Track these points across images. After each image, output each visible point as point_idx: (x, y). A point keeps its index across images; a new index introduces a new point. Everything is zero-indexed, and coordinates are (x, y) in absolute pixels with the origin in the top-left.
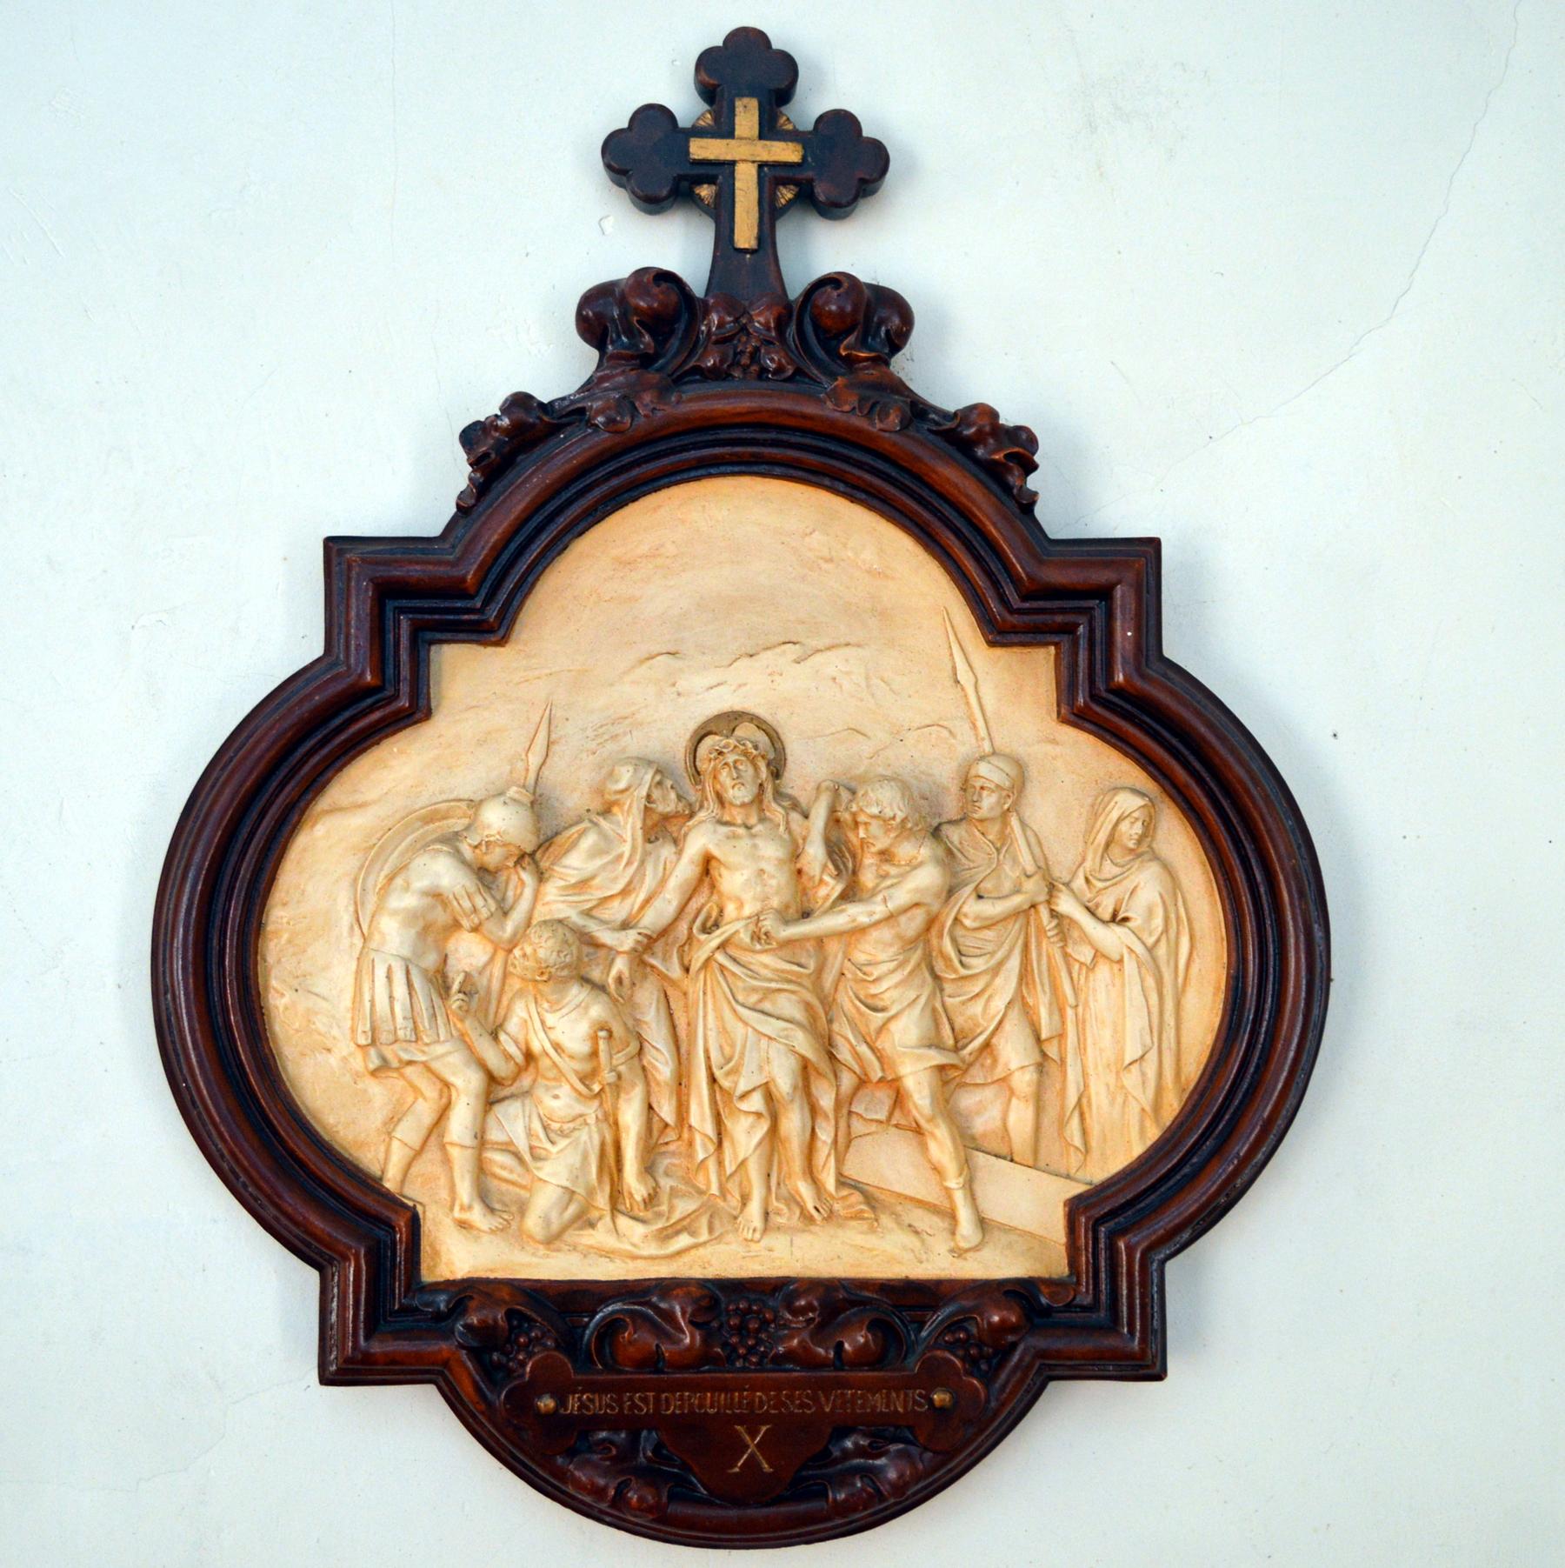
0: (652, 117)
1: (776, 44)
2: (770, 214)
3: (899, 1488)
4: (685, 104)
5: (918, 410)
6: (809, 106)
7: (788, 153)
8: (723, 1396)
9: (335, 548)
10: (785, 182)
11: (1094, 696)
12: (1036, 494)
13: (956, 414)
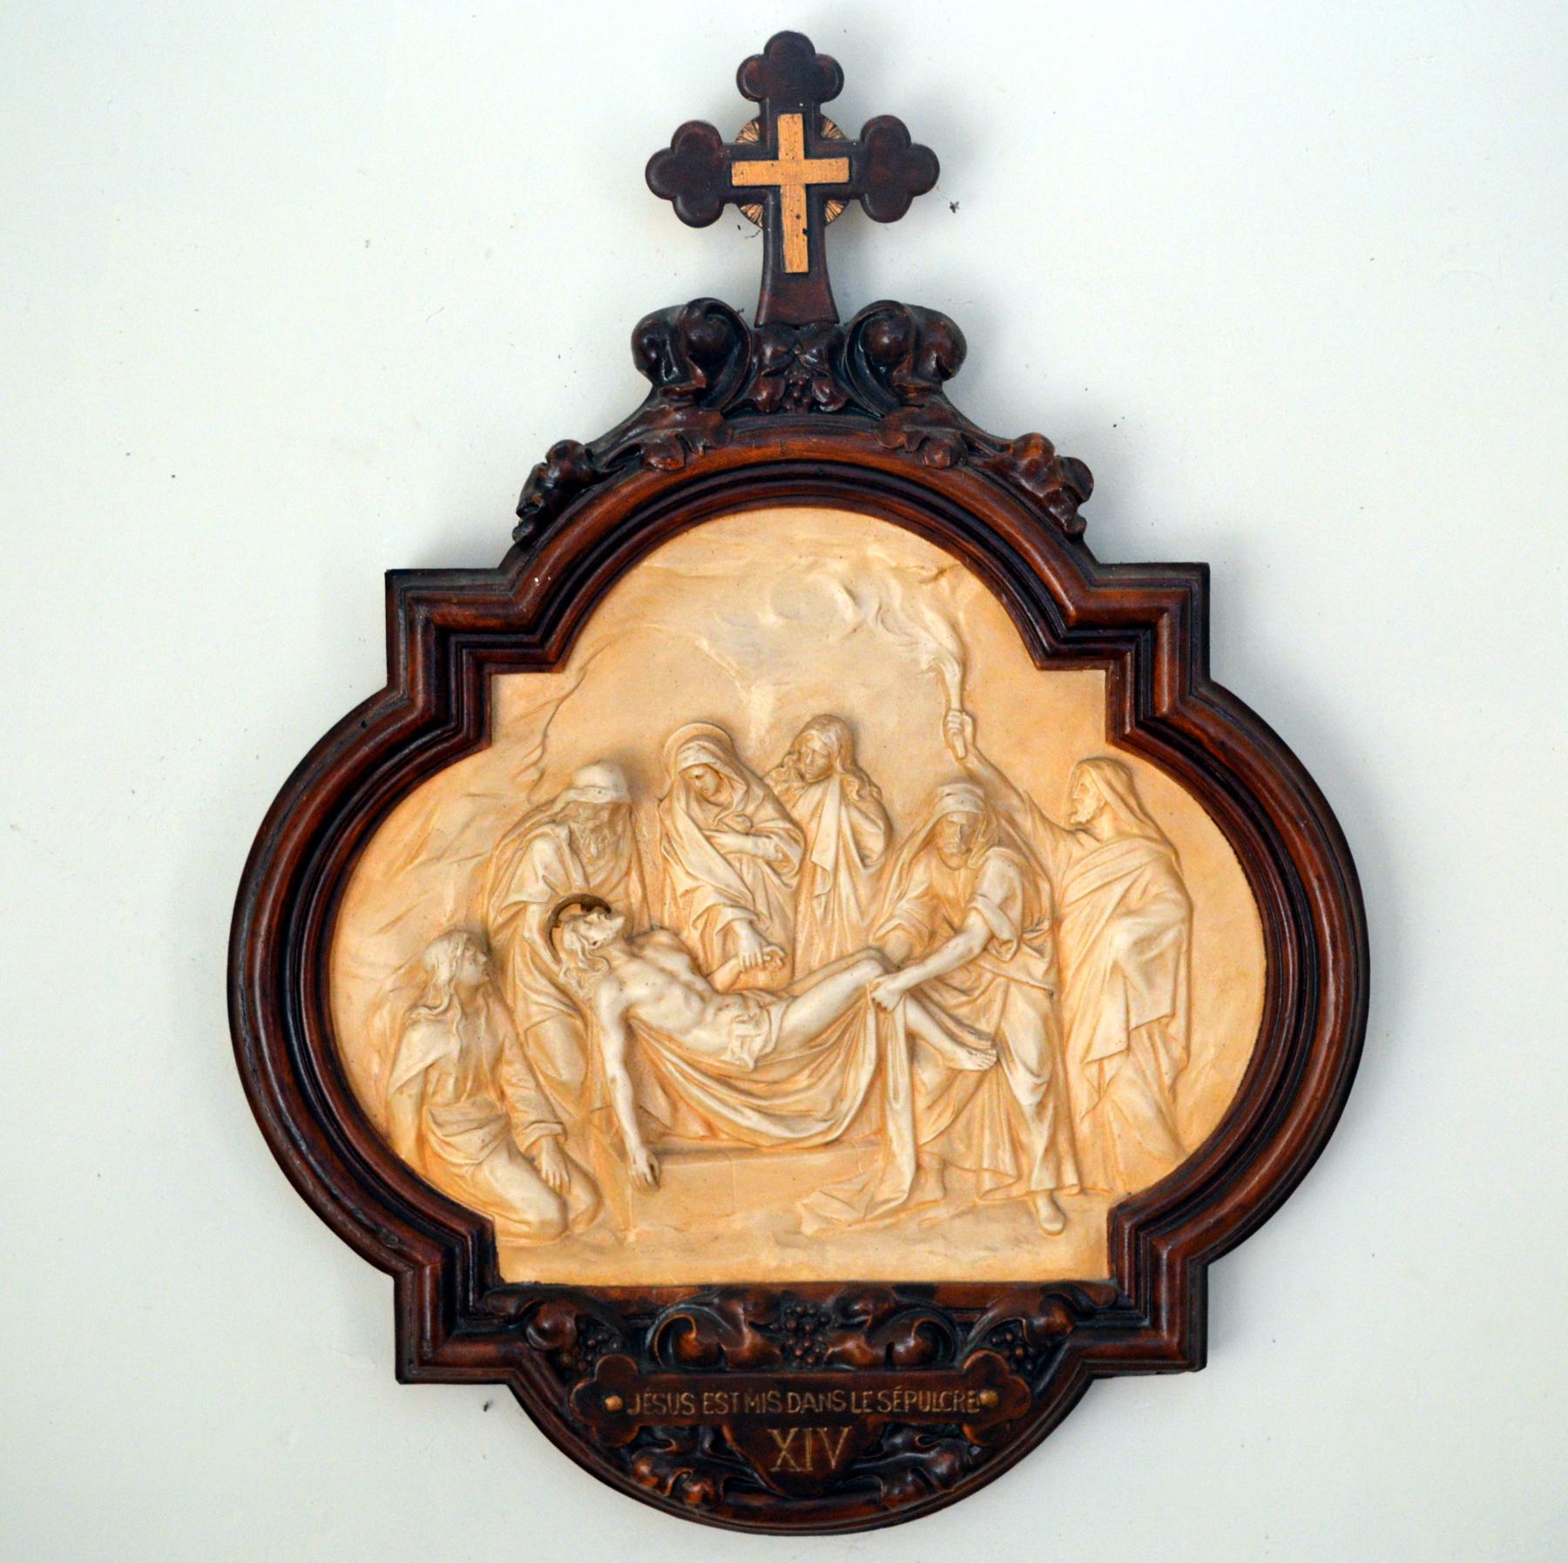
1: (917, 138)
3: (947, 1481)
5: (970, 442)
7: (834, 171)
8: (935, 1395)
11: (1138, 724)
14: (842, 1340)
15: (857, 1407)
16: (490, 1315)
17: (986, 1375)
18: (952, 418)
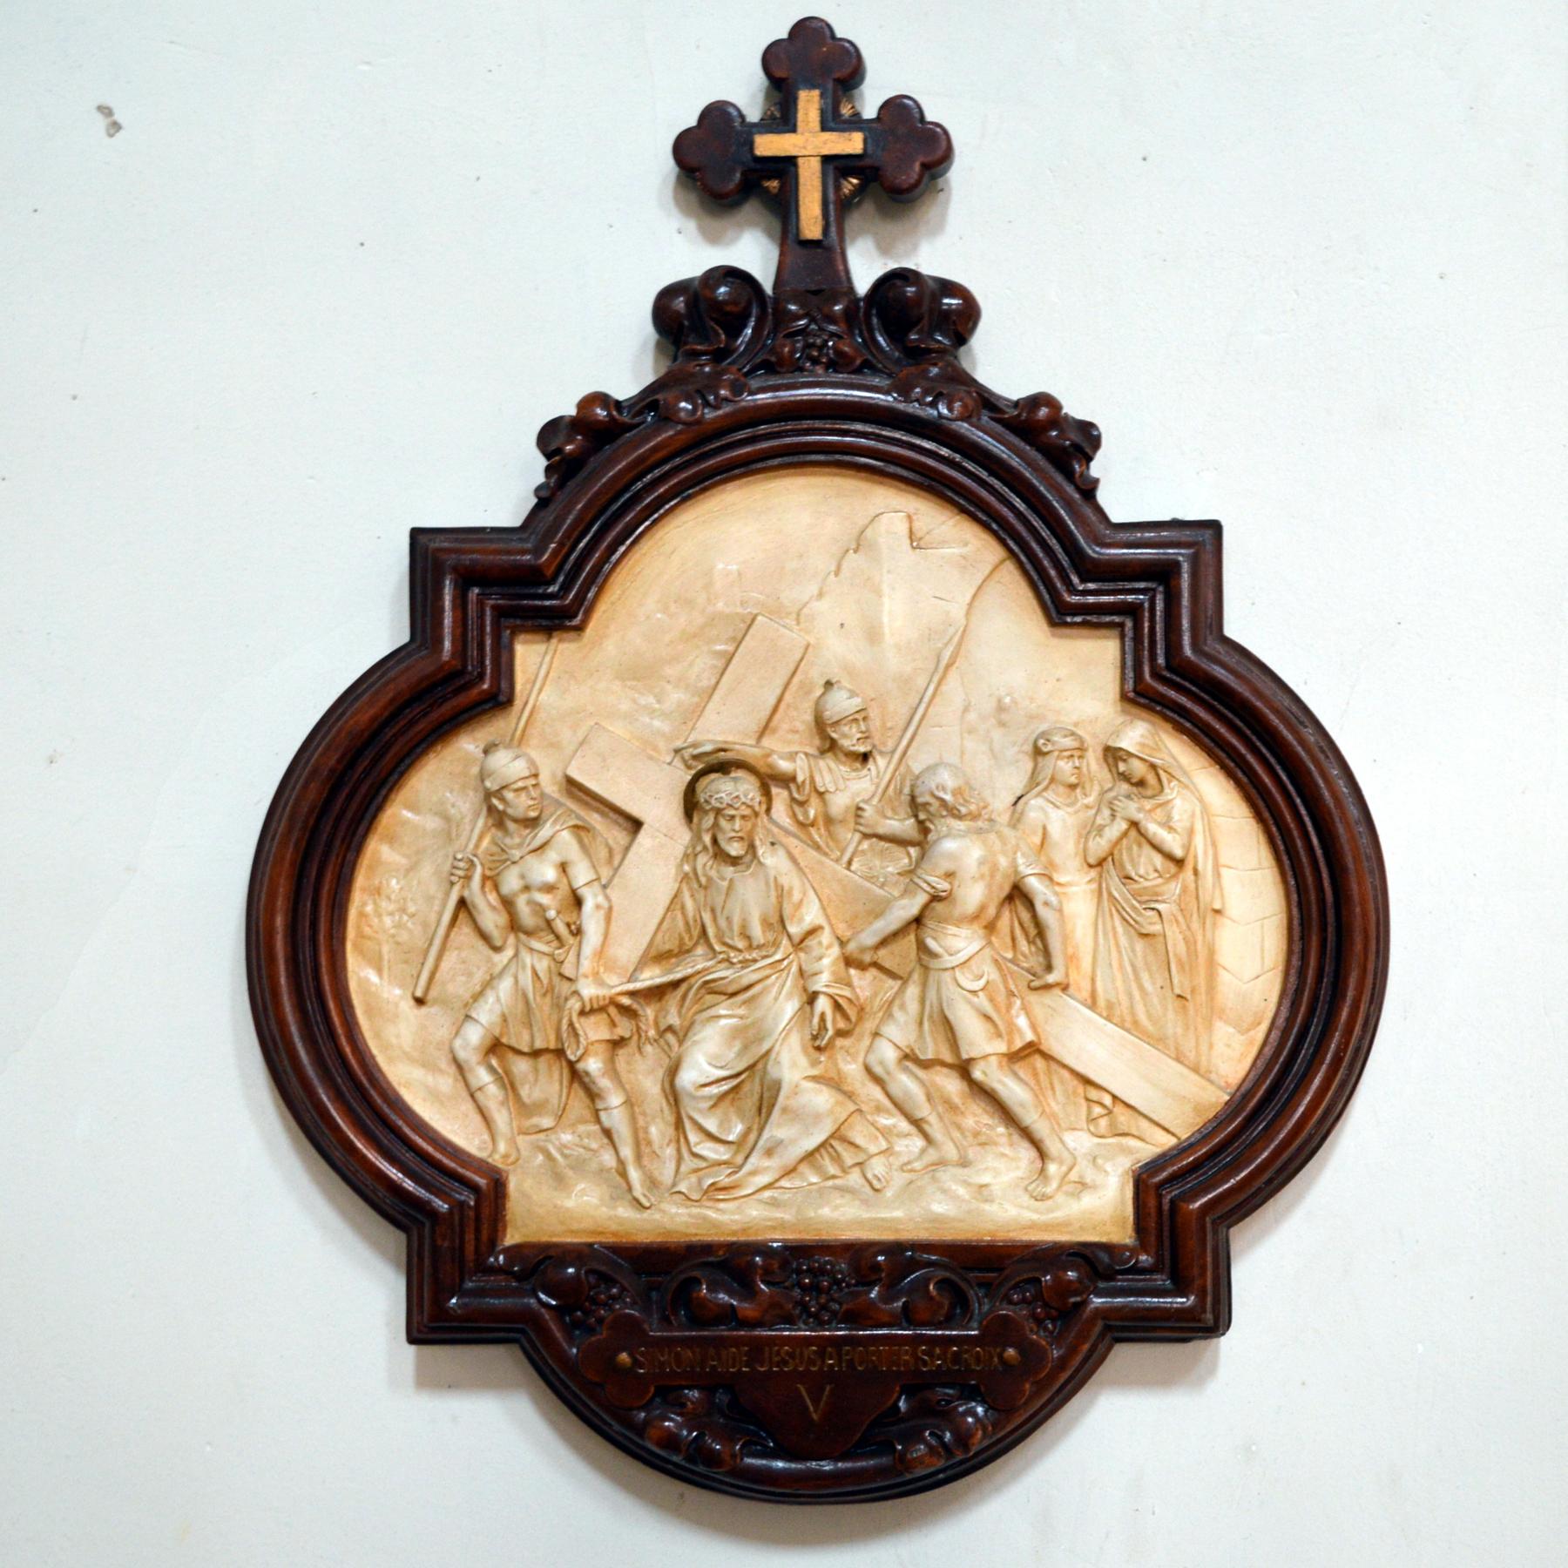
0: (717, 117)
2: (838, 209)
5: (986, 401)
7: (853, 143)
18: (966, 381)
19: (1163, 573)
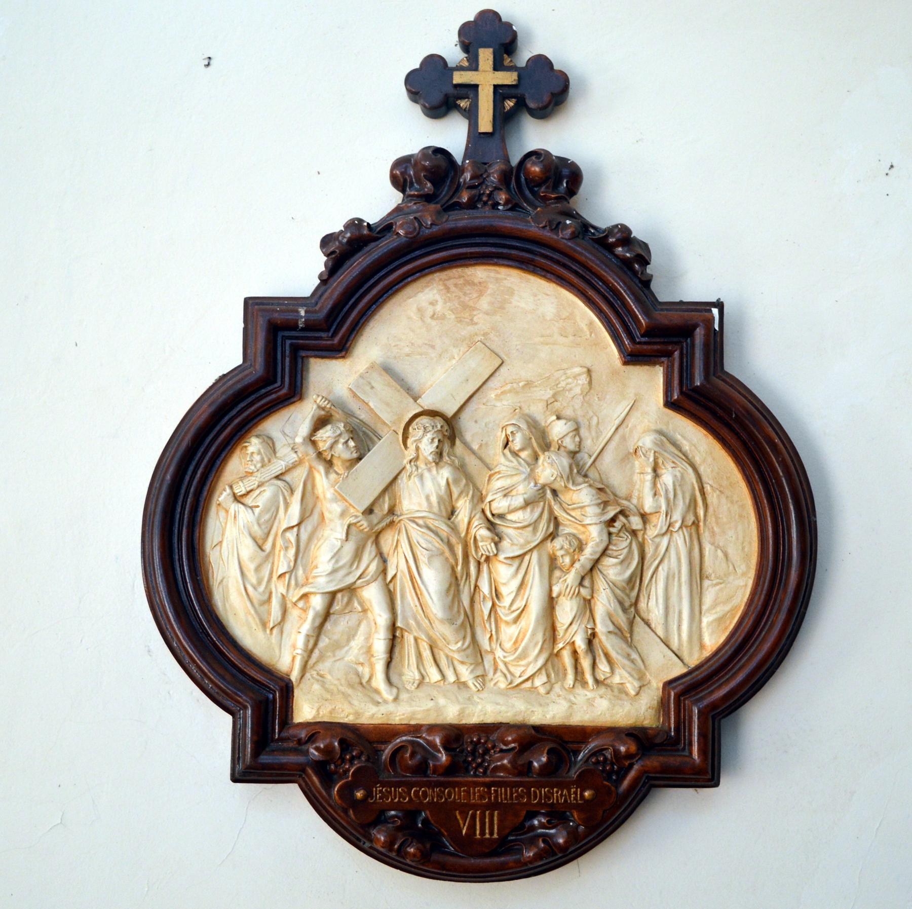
0: (434, 64)
4: (453, 54)
5: (585, 227)
6: (524, 56)
7: (508, 78)
9: (253, 306)
10: (509, 97)
12: (652, 276)
13: (605, 230)
14: (502, 759)
15: (505, 800)
16: (287, 739)
17: (583, 781)
19: (684, 332)
